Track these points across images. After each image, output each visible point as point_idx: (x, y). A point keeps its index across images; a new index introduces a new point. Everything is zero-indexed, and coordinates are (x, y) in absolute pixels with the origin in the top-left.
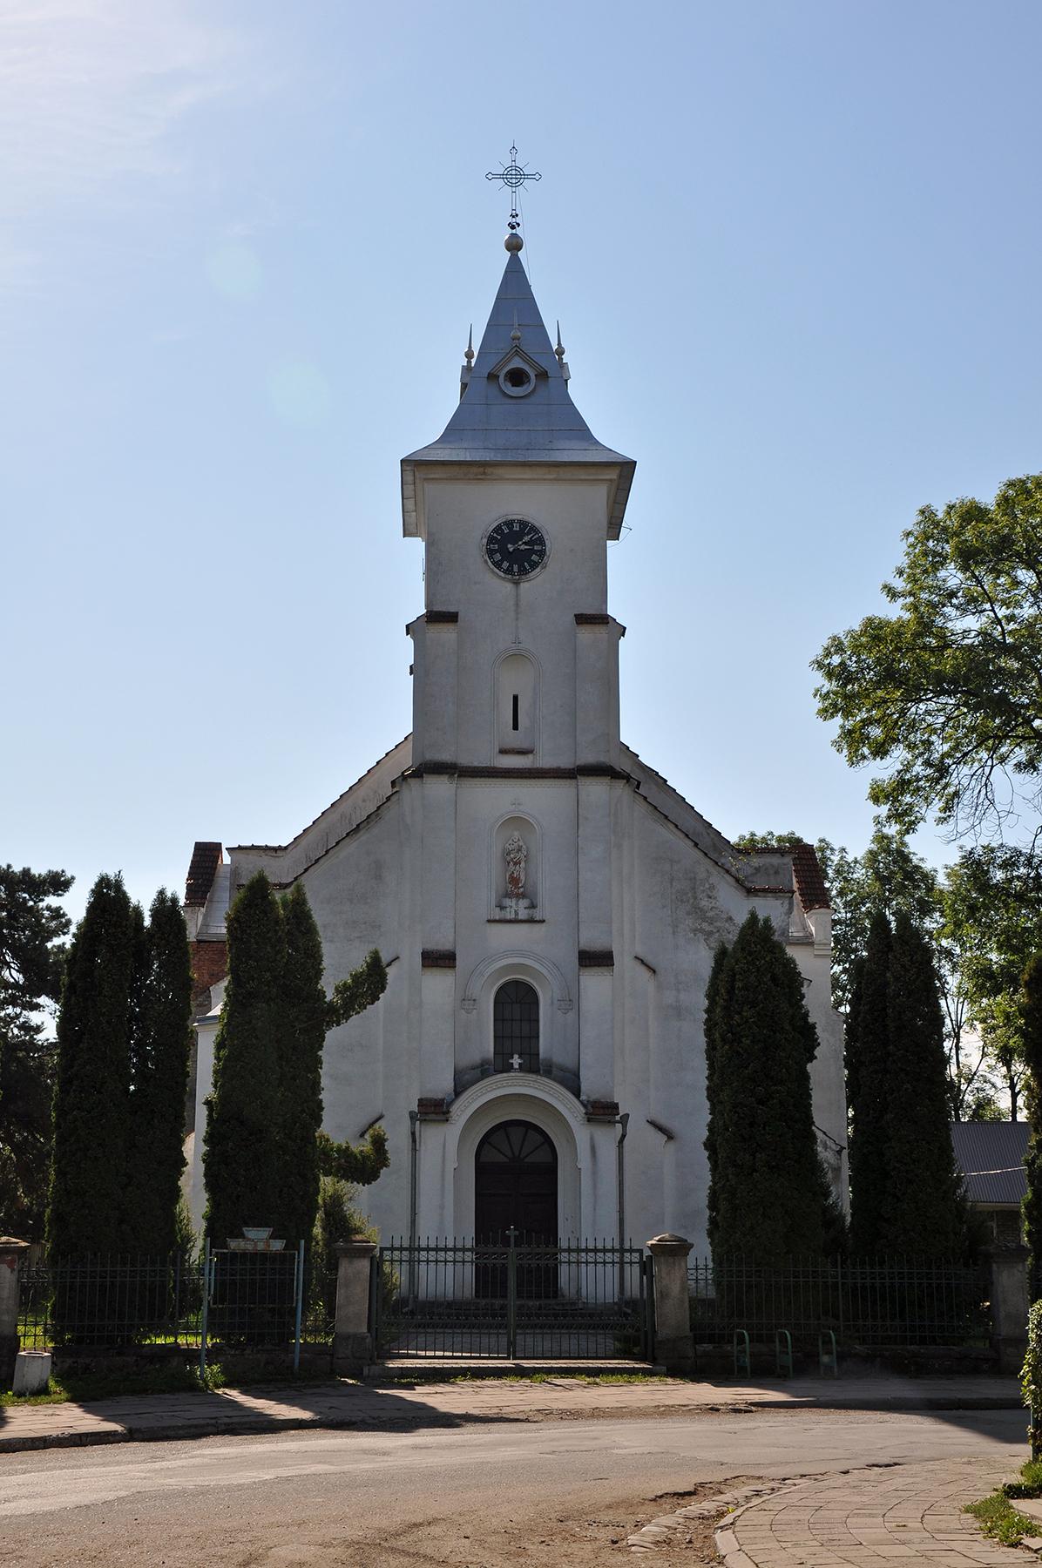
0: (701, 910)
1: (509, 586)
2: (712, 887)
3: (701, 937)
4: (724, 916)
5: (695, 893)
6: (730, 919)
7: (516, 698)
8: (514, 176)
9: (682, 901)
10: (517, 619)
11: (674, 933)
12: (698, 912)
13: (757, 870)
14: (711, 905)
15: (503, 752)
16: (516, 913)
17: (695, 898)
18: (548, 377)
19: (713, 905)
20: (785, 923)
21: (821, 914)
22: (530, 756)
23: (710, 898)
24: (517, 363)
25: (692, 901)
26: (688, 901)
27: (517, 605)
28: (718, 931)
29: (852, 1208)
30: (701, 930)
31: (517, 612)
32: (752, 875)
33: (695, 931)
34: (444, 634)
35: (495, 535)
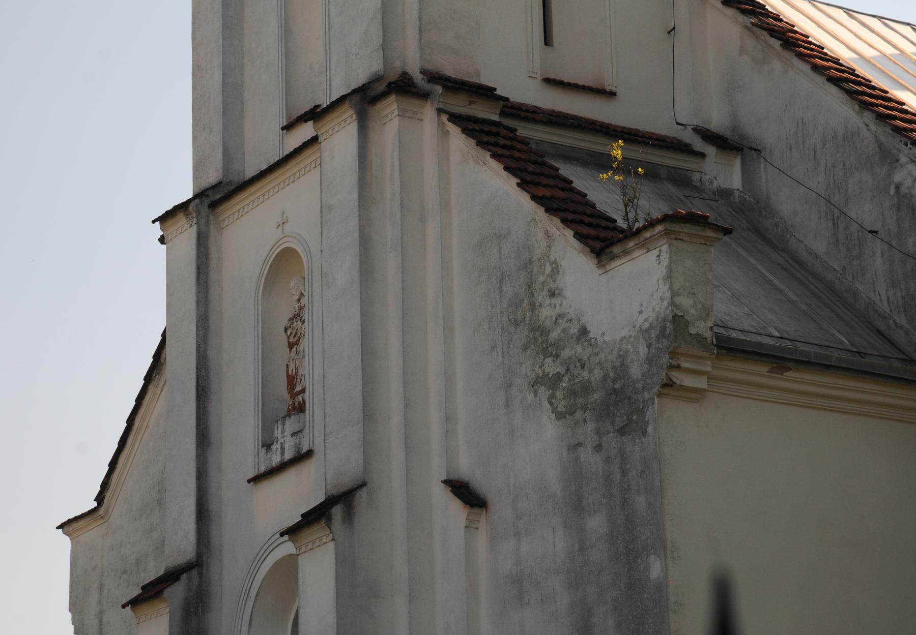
11: (507, 405)
19: (558, 310)
28: (568, 370)
33: (535, 383)
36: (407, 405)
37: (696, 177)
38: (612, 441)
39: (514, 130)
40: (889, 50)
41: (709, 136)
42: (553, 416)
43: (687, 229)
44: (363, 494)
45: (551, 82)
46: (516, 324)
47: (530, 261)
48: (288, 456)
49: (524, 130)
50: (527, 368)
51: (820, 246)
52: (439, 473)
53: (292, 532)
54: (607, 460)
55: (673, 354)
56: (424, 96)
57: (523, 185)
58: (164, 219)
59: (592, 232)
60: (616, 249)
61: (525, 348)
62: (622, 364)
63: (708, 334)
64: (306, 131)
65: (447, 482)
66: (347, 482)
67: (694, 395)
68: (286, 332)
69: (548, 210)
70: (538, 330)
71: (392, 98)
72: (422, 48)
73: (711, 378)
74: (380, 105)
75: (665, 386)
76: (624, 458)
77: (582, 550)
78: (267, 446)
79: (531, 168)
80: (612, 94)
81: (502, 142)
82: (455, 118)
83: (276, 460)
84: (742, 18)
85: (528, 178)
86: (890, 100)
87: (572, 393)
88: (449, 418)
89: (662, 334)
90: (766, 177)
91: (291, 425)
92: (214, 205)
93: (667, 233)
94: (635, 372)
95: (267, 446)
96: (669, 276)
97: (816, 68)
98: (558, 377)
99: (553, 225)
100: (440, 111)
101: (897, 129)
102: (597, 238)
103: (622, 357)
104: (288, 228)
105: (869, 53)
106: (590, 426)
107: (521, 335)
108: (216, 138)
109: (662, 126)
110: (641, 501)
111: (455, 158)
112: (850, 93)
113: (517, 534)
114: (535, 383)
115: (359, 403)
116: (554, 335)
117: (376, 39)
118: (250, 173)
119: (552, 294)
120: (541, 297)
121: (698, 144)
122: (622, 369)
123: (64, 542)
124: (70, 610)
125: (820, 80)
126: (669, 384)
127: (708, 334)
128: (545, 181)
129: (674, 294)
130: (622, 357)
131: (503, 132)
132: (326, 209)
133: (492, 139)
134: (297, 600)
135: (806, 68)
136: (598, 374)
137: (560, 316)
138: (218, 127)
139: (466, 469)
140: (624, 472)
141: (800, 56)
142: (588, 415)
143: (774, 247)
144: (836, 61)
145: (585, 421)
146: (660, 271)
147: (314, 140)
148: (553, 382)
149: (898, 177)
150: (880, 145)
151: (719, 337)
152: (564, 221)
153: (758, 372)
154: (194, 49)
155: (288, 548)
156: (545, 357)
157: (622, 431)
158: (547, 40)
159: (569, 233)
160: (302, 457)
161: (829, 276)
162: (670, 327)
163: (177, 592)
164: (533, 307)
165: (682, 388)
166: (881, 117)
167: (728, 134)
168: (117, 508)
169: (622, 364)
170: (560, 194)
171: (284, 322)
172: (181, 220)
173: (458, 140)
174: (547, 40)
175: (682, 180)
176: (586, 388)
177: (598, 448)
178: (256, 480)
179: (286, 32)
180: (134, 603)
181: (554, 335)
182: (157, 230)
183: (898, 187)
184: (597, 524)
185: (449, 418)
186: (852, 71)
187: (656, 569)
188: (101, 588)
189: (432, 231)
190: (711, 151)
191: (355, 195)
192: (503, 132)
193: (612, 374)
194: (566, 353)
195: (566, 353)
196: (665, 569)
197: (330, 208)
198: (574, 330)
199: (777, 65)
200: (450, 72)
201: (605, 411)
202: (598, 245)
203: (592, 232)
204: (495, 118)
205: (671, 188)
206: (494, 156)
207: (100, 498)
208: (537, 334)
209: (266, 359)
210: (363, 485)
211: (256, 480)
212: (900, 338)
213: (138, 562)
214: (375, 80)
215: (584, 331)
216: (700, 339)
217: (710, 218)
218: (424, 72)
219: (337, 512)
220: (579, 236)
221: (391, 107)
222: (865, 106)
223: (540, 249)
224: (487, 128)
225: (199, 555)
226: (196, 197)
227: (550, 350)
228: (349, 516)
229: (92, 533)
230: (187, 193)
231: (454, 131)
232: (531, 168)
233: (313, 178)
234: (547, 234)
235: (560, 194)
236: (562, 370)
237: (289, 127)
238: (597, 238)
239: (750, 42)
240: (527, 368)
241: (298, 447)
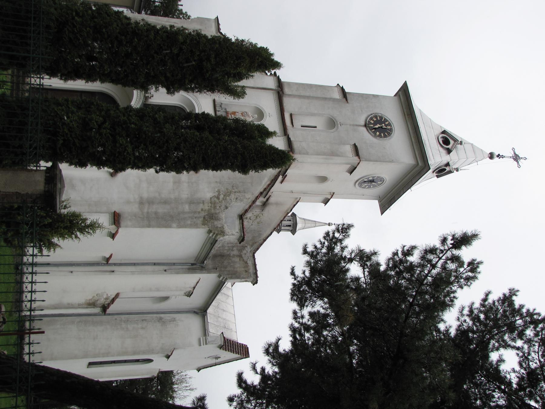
0: (229, 195)
1: (363, 123)
2: (242, 201)
3: (216, 194)
4: (228, 205)
5: (238, 192)
6: (227, 208)
7: (315, 127)
8: (516, 158)
9: (233, 186)
10: (350, 125)
11: (216, 182)
12: (228, 194)
13: (246, 263)
14: (232, 199)
15: (291, 115)
16: (219, 111)
17: (235, 192)
18: (449, 154)
19: (233, 200)
20: (227, 233)
21: (221, 339)
22: (291, 126)
23: (236, 199)
24: (452, 142)
25: (234, 191)
26: (233, 189)
27: (357, 125)
28: (220, 202)
29: (94, 80)
30: (219, 194)
31: (353, 125)
32: (244, 260)
33: (219, 191)
34: (337, 95)
35: (383, 119)
38: (203, 214)
41: (268, 199)
42: (211, 197)
47: (245, 192)
50: (223, 189)
62: (218, 219)
68: (245, 112)
93: (241, 236)
134: (37, 364)
142: (209, 207)
145: (208, 206)
156: (224, 195)
157: (204, 218)
169: (218, 219)
183: (247, 246)
190: (265, 200)
193: (216, 216)
208: (229, 193)
217: (262, 172)
225: (108, 213)
236: (220, 201)
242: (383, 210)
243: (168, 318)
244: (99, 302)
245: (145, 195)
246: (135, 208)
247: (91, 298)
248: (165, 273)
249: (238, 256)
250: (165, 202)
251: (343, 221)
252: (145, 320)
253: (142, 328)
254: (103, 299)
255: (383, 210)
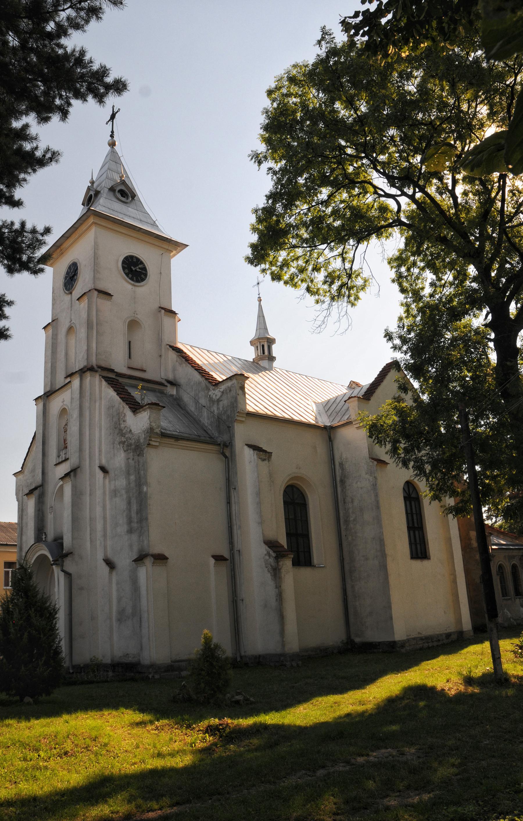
1: (70, 296)
13: (223, 392)
32: (221, 396)
33: (120, 443)
36: (90, 448)
37: (165, 391)
38: (136, 458)
39: (118, 380)
40: (217, 361)
43: (154, 406)
44: (79, 469)
45: (130, 368)
46: (116, 428)
48: (63, 459)
49: (121, 380)
50: (118, 439)
51: (193, 409)
52: (97, 464)
53: (62, 479)
54: (135, 462)
55: (150, 437)
56: (96, 371)
57: (118, 394)
58: (36, 400)
59: (133, 406)
60: (138, 411)
61: (118, 434)
63: (159, 432)
64: (68, 380)
65: (99, 467)
66: (75, 466)
67: (156, 447)
69: (123, 401)
70: (121, 430)
71: (88, 372)
72: (96, 360)
73: (159, 442)
74: (86, 373)
75: (148, 445)
76: (139, 462)
77: (129, 484)
78: (59, 456)
79: (120, 390)
80: (145, 371)
81: (114, 383)
82: (104, 377)
83: (61, 460)
84: (176, 353)
85: (119, 392)
86: (209, 374)
87: (128, 446)
88: (100, 451)
89: (147, 432)
90: (181, 392)
91: (64, 452)
92: (48, 396)
93: (149, 408)
94: (142, 441)
95: (59, 456)
96: (150, 418)
97: (192, 366)
98: (125, 442)
99: (124, 404)
100: (100, 375)
101: (210, 382)
102: (134, 408)
103: (139, 437)
104: (65, 403)
105: (211, 362)
106: (132, 454)
107: (117, 431)
108: (49, 379)
109: (157, 379)
110: (142, 472)
111: (103, 387)
112: (200, 373)
113: (115, 480)
114: (120, 443)
115: (78, 447)
116: (124, 431)
117: (85, 357)
118: (57, 389)
119: (124, 421)
120: (121, 422)
121: (166, 384)
122: (139, 440)
123: (14, 478)
124: (387, 364)
125: (193, 369)
126: (149, 444)
127: (159, 432)
128: (123, 393)
129: (150, 422)
130: (139, 437)
131: (115, 381)
132: (72, 399)
133: (112, 383)
135: (190, 366)
136: (133, 441)
137: (125, 427)
138: (50, 377)
139: (104, 462)
140: (139, 465)
141: (189, 363)
142: (131, 451)
143: (181, 408)
144: (198, 365)
146: (147, 417)
147: (70, 382)
148: (123, 443)
149: (210, 393)
150: (206, 385)
151: (162, 432)
152: (126, 404)
153: (172, 441)
154: (45, 358)
155: (61, 483)
157: (138, 455)
158: (130, 357)
159: (128, 407)
160: (66, 460)
161: (195, 416)
162: (149, 430)
163: (37, 492)
164: (120, 424)
165: (152, 445)
166: (206, 379)
167: (173, 381)
168: (26, 471)
170: (126, 396)
171: (63, 426)
172: (40, 400)
173: (104, 383)
174: (130, 357)
175: (162, 392)
176: (131, 445)
177: (133, 459)
178: (56, 465)
179: (67, 354)
180: (27, 495)
181: (124, 431)
182: (34, 402)
184: (132, 477)
185: (100, 451)
186: (201, 367)
187: (145, 489)
188: (22, 490)
189: (97, 404)
190: (169, 385)
191: (79, 396)
192: (115, 381)
194: (127, 436)
195: (127, 436)
196: (147, 489)
197: (73, 399)
198: (128, 430)
199: (184, 365)
200: (103, 366)
201: (135, 450)
202: (134, 410)
203: (133, 406)
204: (114, 377)
205: (159, 394)
206: (112, 387)
207: (22, 468)
209: (59, 435)
210: (79, 467)
211: (56, 465)
212: (209, 432)
213: (31, 484)
214: (85, 367)
215: (131, 431)
216: (157, 433)
218: (97, 365)
219: (72, 474)
220: (130, 408)
221: (88, 374)
222: (203, 376)
223: (121, 410)
224: (111, 380)
226: (44, 394)
227: (123, 435)
228: (75, 476)
229: (21, 477)
230: (42, 393)
231: (103, 380)
232: (120, 390)
233: (69, 391)
234: (123, 407)
235: (126, 396)
237: (66, 378)
238: (134, 408)
239: (178, 359)
240: (118, 439)
241: (65, 457)
242: (179, 246)
243: (340, 472)
244: (273, 564)
245: (125, 528)
246: (134, 537)
247: (269, 575)
248: (237, 489)
249: (218, 404)
250: (129, 503)
251: (255, 286)
252: (344, 500)
253: (352, 502)
254: (270, 560)
255: (179, 246)
